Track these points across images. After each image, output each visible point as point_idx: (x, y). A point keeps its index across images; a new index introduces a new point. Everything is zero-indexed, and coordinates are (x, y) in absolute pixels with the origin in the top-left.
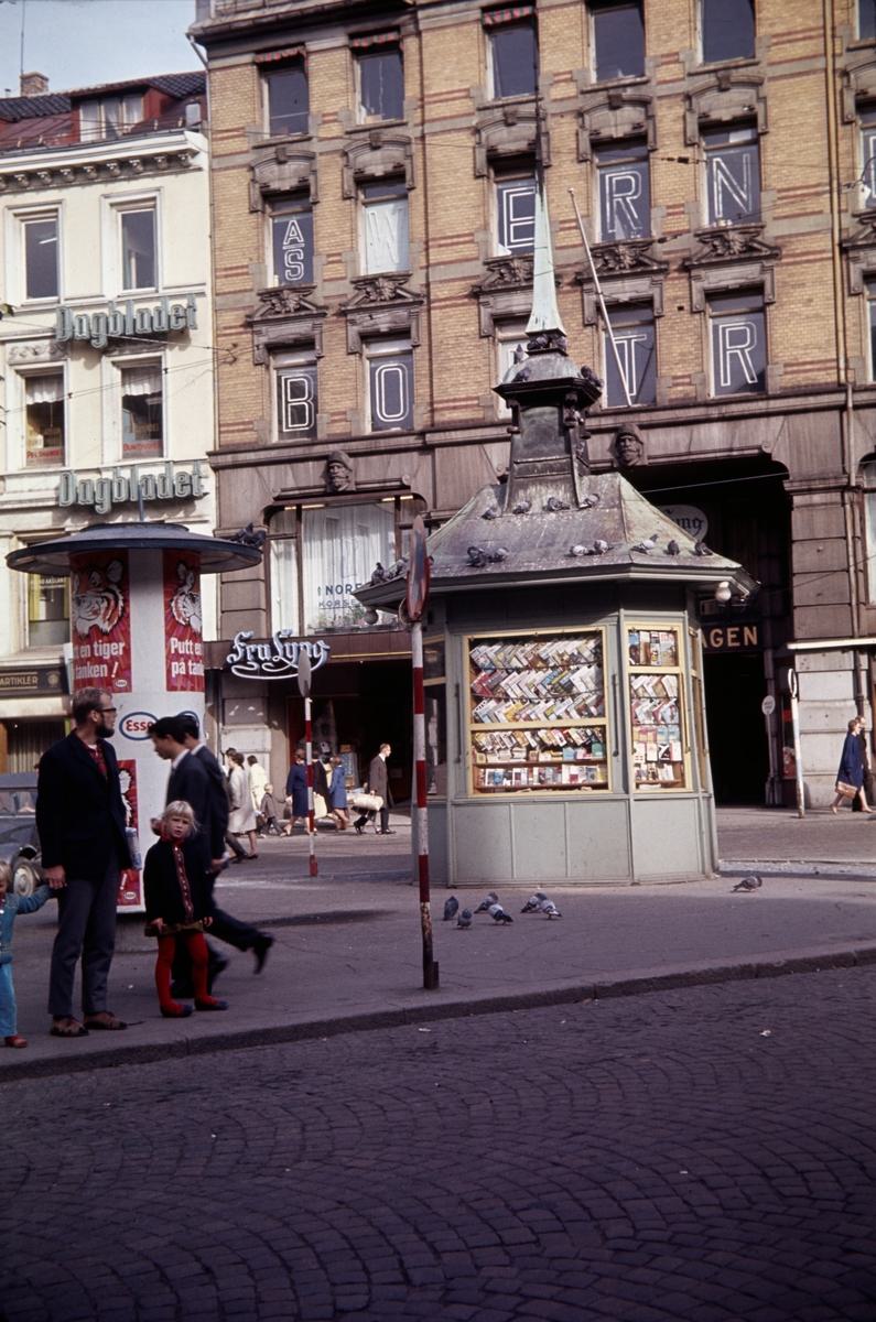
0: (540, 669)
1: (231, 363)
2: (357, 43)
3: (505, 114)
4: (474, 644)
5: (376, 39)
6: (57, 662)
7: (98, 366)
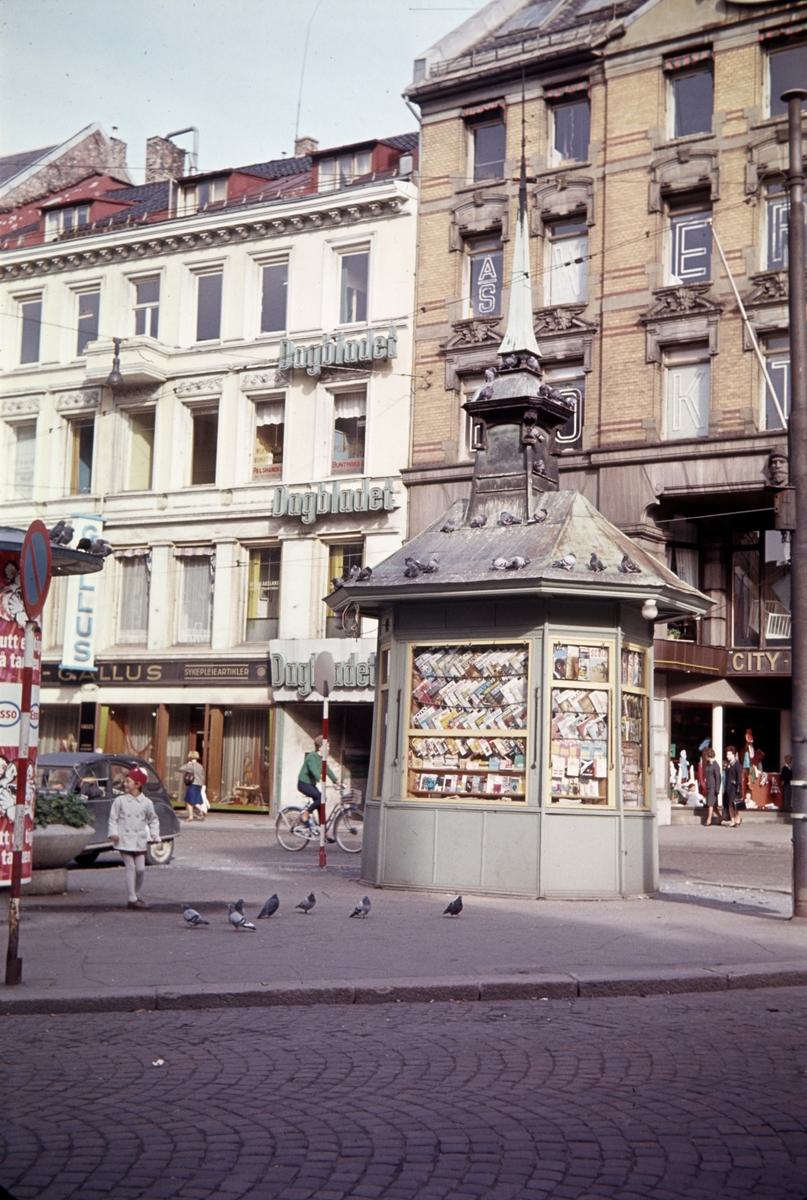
0: (475, 679)
1: (426, 389)
2: (550, 94)
3: (678, 153)
4: (418, 652)
5: (568, 89)
6: (265, 656)
7: (314, 392)
